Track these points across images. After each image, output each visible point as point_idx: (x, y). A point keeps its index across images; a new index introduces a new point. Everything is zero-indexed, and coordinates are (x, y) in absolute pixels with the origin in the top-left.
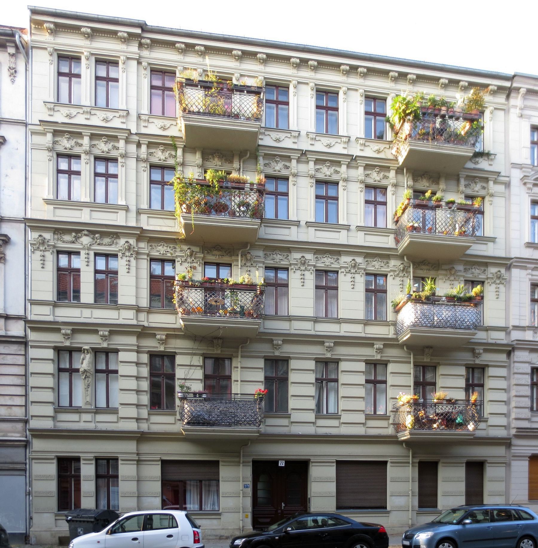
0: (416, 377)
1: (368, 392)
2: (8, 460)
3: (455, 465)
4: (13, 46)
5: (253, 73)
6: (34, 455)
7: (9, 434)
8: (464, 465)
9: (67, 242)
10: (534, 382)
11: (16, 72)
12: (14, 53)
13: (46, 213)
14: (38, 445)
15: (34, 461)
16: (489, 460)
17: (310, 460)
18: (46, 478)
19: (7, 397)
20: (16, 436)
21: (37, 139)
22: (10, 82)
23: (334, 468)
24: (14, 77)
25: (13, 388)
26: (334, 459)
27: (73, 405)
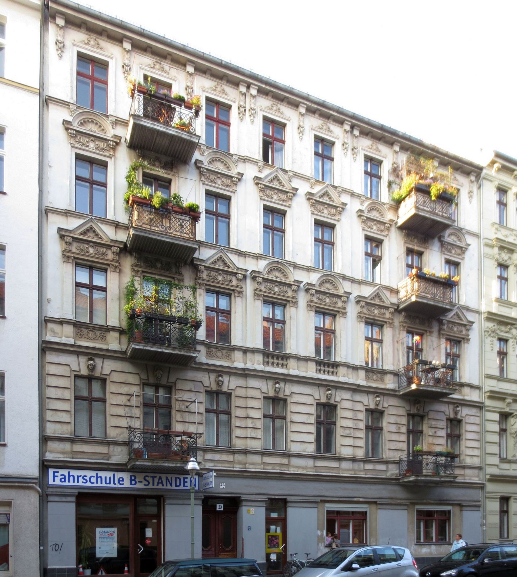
0: (318, 417)
1: (266, 429)
2: (471, 499)
3: (492, 500)
4: (255, 89)
5: (202, 88)
6: (488, 495)
7: (473, 478)
8: (498, 500)
9: (502, 331)
10: (369, 426)
11: (64, 46)
12: (130, 49)
13: (495, 308)
14: (490, 487)
15: (487, 500)
16: (243, 497)
17: (240, 497)
18: (492, 513)
19: (471, 449)
20: (475, 480)
21: (488, 250)
22: (57, 58)
23: (72, 507)
24: (62, 52)
25: (473, 442)
26: (499, 495)
27: (93, 436)
